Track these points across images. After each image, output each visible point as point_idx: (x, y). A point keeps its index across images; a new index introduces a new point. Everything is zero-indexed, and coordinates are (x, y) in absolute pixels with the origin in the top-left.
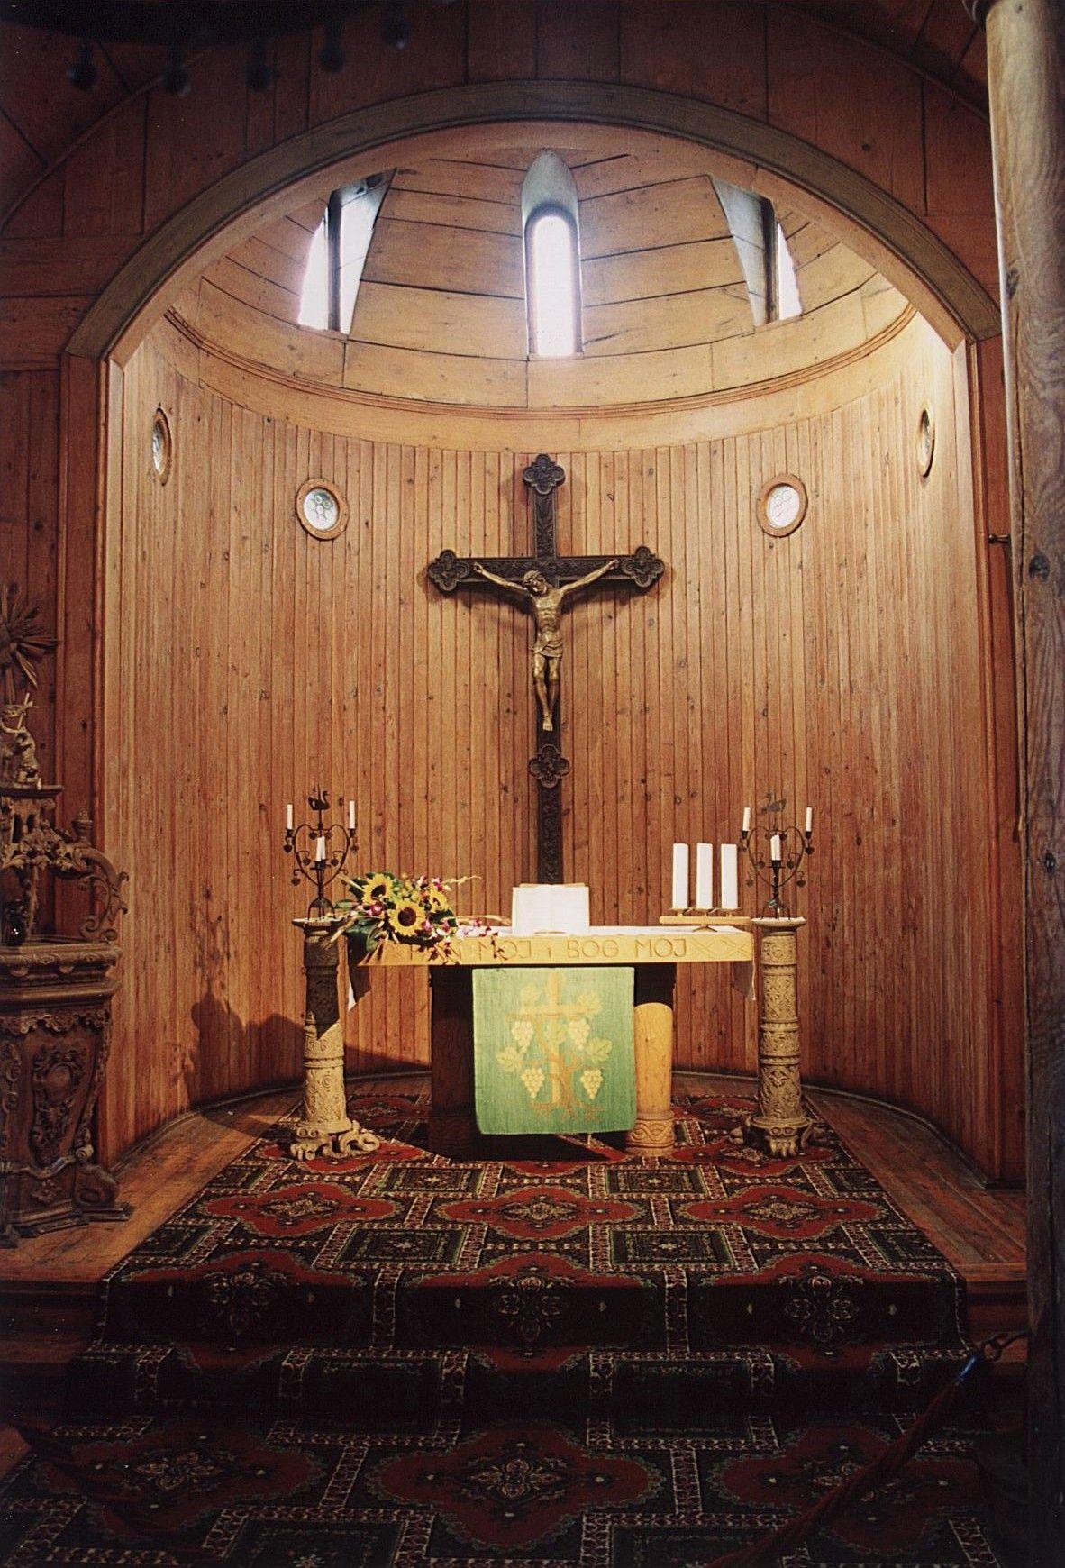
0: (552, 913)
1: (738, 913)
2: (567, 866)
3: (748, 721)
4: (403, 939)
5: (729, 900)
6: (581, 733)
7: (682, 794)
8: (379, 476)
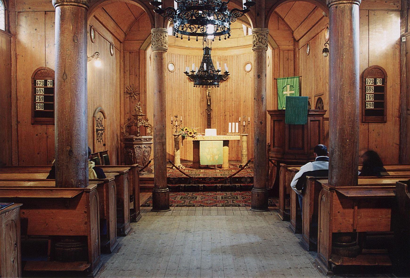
0: (211, 133)
1: (238, 133)
2: (212, 127)
3: (242, 103)
4: (190, 137)
5: (237, 131)
6: (214, 104)
7: (231, 115)
8: (181, 60)
